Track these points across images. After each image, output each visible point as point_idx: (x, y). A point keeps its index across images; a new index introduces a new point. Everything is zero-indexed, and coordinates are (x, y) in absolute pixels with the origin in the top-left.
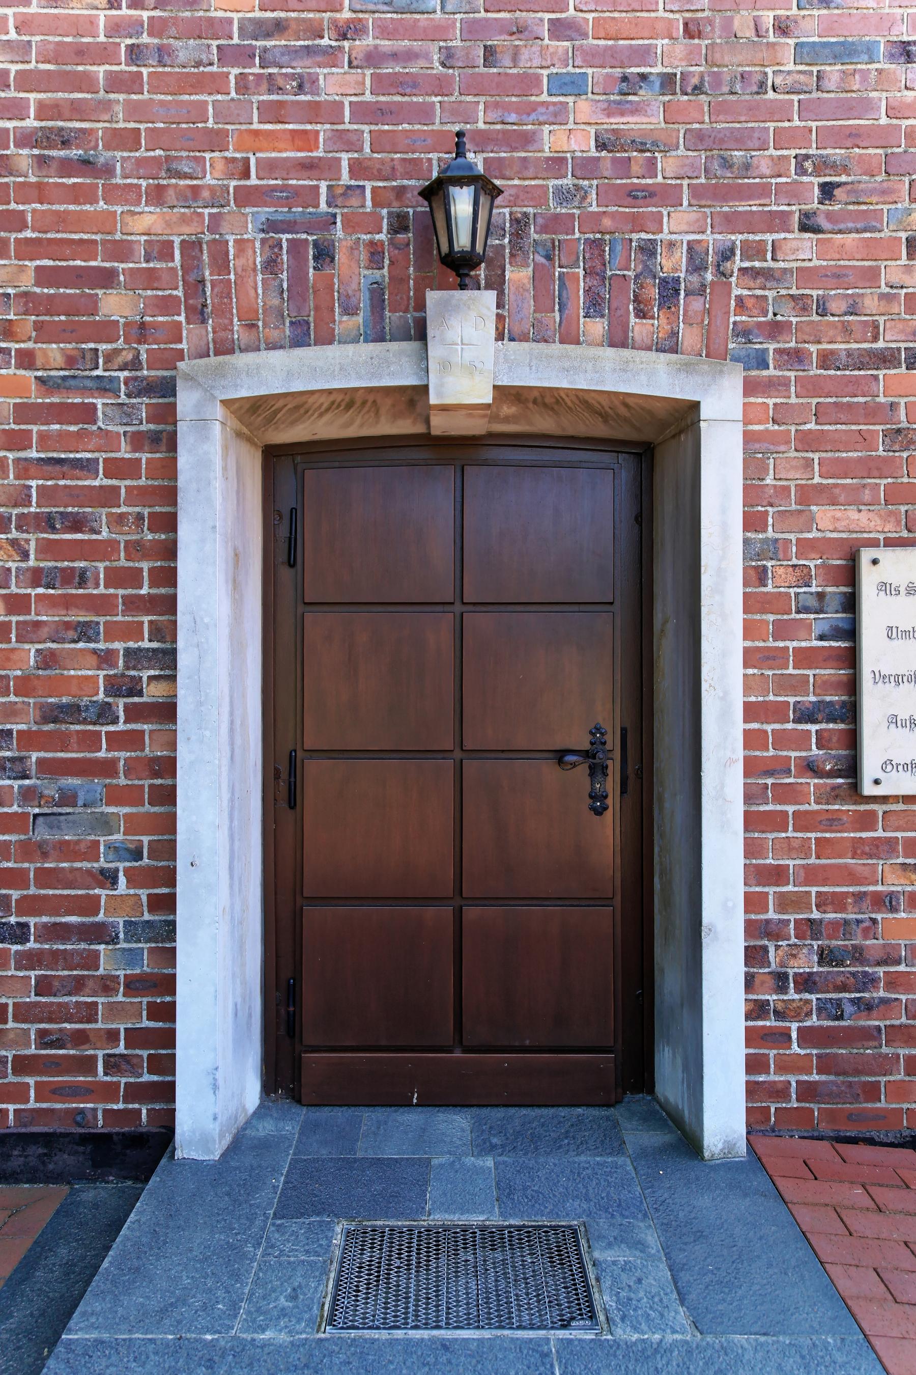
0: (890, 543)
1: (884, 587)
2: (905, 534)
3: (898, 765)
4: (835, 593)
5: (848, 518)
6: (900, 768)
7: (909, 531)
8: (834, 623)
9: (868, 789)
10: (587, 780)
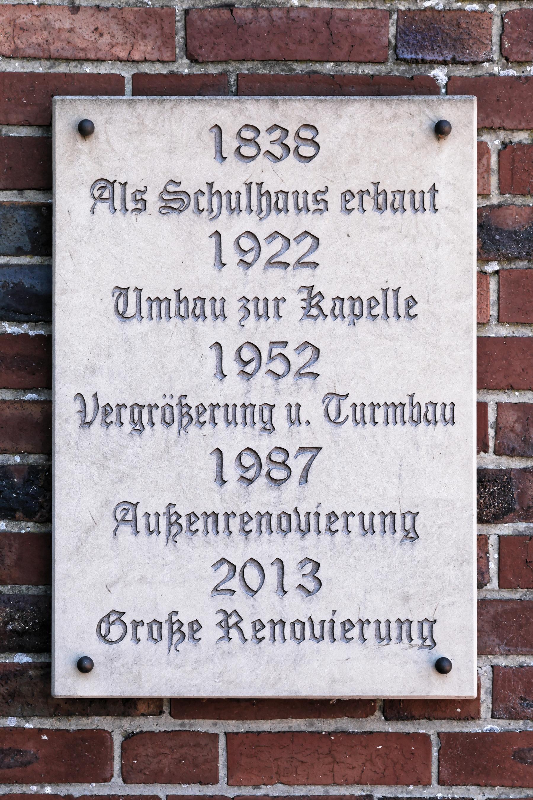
0: (148, 87)
1: (104, 189)
2: (183, 67)
3: (137, 624)
4: (13, 206)
5: (47, 26)
6: (143, 632)
7: (194, 60)
8: (12, 280)
9: (67, 684)
10: (490, 538)
